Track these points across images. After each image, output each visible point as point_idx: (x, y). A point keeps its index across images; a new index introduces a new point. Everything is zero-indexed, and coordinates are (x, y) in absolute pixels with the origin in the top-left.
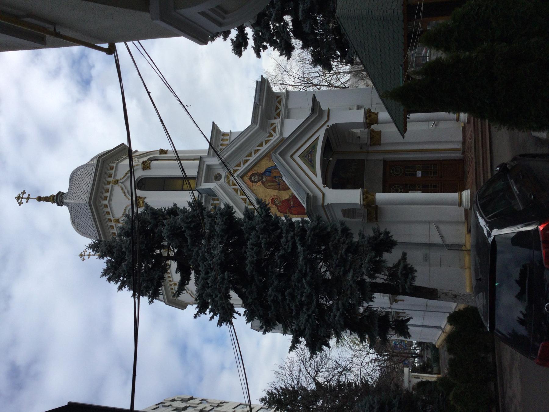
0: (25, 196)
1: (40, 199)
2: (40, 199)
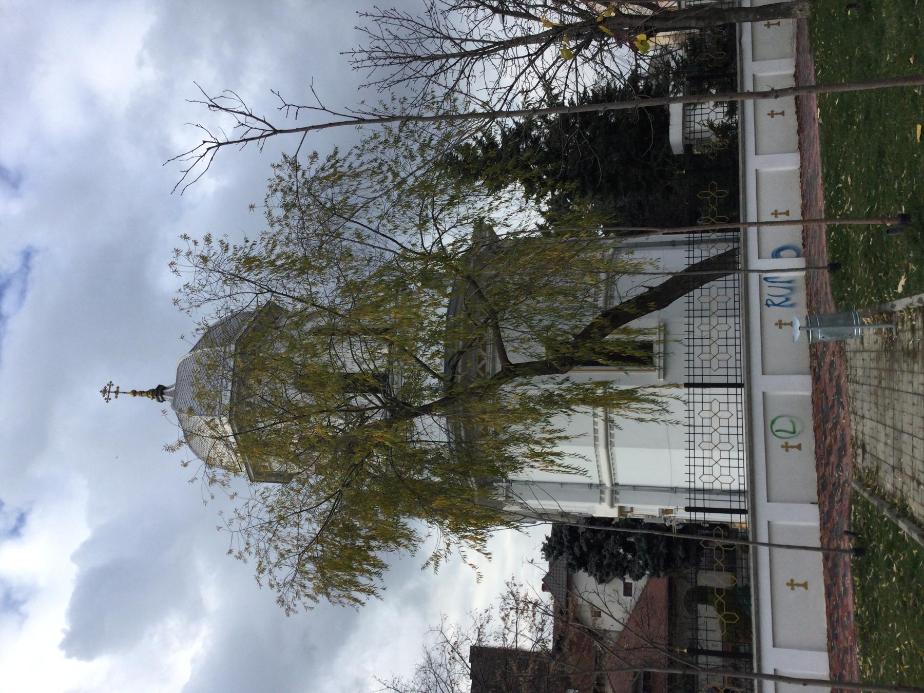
0: (113, 389)
1: (134, 393)
2: (134, 393)
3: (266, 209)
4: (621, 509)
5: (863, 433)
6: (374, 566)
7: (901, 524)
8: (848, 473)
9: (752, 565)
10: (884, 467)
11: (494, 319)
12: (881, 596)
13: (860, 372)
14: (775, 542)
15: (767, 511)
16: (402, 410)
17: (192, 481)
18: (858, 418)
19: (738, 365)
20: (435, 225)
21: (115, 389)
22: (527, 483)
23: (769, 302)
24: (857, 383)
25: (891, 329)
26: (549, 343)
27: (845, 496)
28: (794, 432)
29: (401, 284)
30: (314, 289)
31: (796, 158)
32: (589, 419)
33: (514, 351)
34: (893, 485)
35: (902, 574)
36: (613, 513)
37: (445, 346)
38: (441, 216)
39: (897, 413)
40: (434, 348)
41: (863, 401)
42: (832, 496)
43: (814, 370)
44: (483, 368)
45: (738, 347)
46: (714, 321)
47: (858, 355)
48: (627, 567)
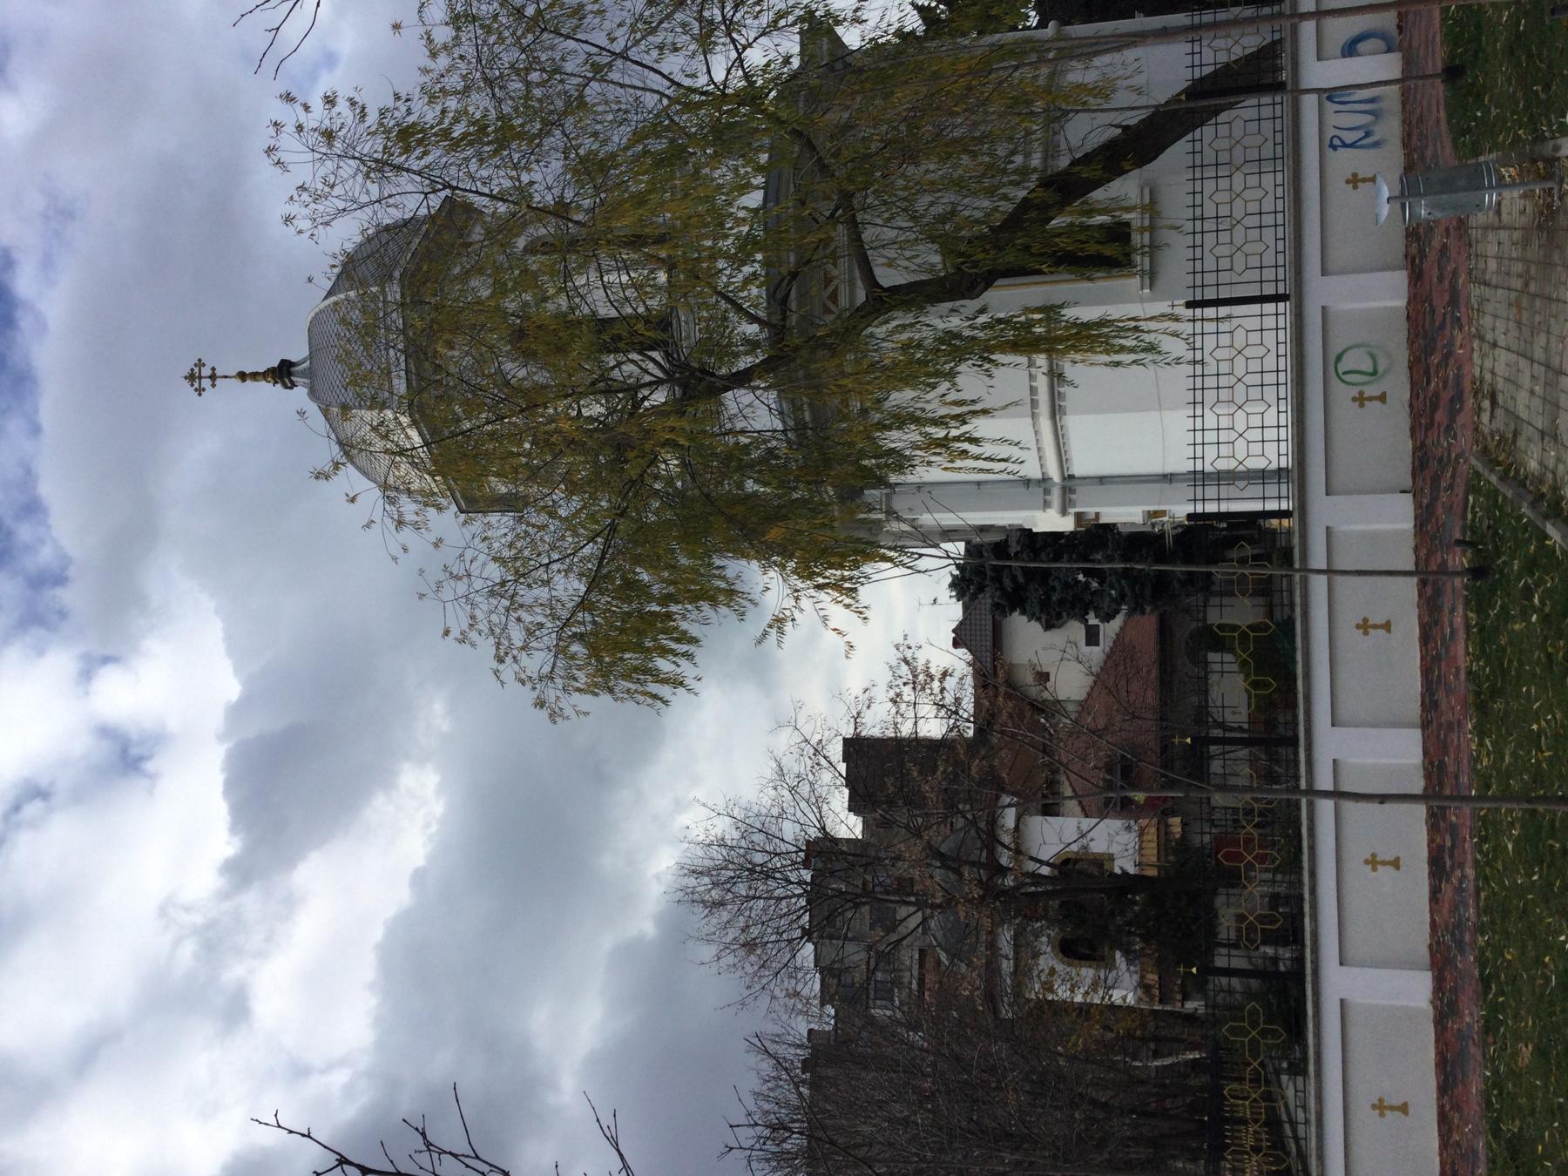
0: (206, 372)
1: (242, 376)
2: (242, 376)
3: (422, 30)
4: (1079, 517)
5: (1493, 373)
6: (678, 640)
7: (1550, 530)
8: (1464, 441)
9: (1298, 600)
10: (1528, 431)
11: (848, 211)
12: (1511, 643)
13: (1492, 265)
14: (1346, 788)
15: (1326, 512)
16: (699, 383)
17: (368, 526)
18: (1486, 347)
19: (1281, 262)
20: (729, 35)
21: (209, 373)
22: (920, 486)
23: (1337, 142)
24: (1486, 284)
25: (1551, 189)
26: (947, 246)
27: (1458, 480)
28: (1375, 373)
29: (677, 155)
30: (525, 178)
32: (1021, 376)
33: (889, 265)
34: (1541, 463)
35: (1547, 610)
36: (1066, 525)
37: (766, 263)
38: (738, 15)
39: (1553, 339)
40: (747, 270)
41: (1495, 317)
42: (1436, 480)
43: (1413, 261)
44: (834, 297)
45: (1280, 229)
46: (1238, 178)
47: (1490, 236)
48: (1091, 602)
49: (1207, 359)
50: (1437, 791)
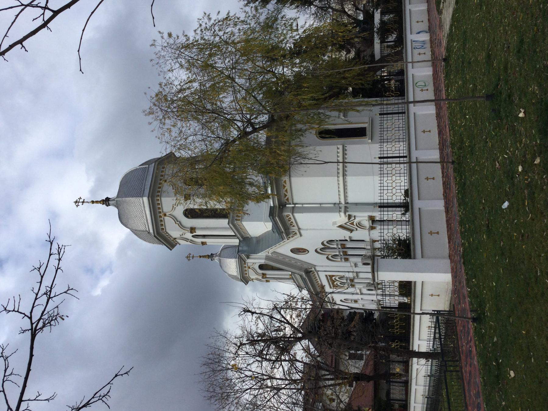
1: (93, 202)
2: (93, 202)
14: (414, 61)
31: (426, 4)
46: (394, 178)
49: (385, 235)
50: (443, 161)
